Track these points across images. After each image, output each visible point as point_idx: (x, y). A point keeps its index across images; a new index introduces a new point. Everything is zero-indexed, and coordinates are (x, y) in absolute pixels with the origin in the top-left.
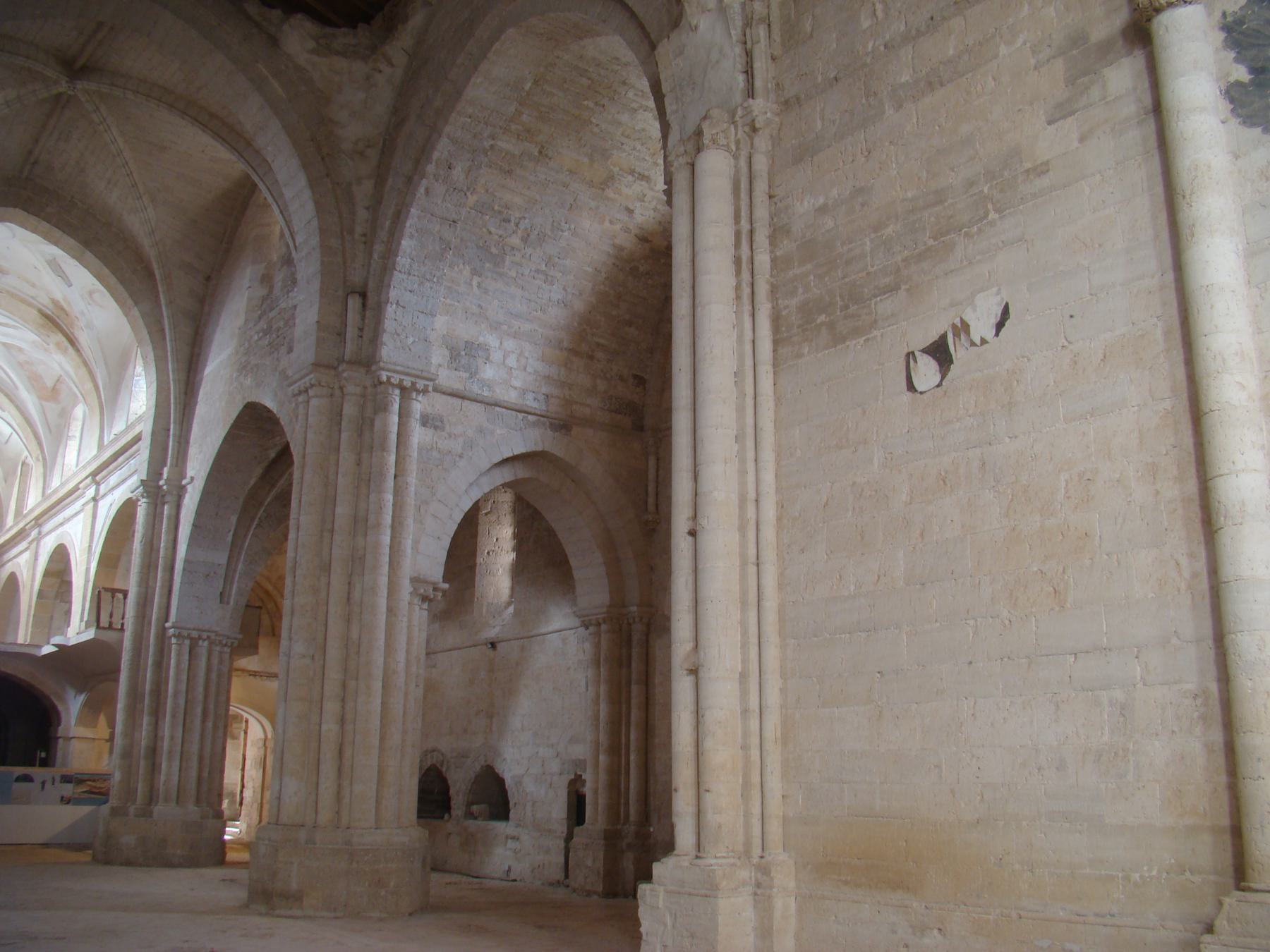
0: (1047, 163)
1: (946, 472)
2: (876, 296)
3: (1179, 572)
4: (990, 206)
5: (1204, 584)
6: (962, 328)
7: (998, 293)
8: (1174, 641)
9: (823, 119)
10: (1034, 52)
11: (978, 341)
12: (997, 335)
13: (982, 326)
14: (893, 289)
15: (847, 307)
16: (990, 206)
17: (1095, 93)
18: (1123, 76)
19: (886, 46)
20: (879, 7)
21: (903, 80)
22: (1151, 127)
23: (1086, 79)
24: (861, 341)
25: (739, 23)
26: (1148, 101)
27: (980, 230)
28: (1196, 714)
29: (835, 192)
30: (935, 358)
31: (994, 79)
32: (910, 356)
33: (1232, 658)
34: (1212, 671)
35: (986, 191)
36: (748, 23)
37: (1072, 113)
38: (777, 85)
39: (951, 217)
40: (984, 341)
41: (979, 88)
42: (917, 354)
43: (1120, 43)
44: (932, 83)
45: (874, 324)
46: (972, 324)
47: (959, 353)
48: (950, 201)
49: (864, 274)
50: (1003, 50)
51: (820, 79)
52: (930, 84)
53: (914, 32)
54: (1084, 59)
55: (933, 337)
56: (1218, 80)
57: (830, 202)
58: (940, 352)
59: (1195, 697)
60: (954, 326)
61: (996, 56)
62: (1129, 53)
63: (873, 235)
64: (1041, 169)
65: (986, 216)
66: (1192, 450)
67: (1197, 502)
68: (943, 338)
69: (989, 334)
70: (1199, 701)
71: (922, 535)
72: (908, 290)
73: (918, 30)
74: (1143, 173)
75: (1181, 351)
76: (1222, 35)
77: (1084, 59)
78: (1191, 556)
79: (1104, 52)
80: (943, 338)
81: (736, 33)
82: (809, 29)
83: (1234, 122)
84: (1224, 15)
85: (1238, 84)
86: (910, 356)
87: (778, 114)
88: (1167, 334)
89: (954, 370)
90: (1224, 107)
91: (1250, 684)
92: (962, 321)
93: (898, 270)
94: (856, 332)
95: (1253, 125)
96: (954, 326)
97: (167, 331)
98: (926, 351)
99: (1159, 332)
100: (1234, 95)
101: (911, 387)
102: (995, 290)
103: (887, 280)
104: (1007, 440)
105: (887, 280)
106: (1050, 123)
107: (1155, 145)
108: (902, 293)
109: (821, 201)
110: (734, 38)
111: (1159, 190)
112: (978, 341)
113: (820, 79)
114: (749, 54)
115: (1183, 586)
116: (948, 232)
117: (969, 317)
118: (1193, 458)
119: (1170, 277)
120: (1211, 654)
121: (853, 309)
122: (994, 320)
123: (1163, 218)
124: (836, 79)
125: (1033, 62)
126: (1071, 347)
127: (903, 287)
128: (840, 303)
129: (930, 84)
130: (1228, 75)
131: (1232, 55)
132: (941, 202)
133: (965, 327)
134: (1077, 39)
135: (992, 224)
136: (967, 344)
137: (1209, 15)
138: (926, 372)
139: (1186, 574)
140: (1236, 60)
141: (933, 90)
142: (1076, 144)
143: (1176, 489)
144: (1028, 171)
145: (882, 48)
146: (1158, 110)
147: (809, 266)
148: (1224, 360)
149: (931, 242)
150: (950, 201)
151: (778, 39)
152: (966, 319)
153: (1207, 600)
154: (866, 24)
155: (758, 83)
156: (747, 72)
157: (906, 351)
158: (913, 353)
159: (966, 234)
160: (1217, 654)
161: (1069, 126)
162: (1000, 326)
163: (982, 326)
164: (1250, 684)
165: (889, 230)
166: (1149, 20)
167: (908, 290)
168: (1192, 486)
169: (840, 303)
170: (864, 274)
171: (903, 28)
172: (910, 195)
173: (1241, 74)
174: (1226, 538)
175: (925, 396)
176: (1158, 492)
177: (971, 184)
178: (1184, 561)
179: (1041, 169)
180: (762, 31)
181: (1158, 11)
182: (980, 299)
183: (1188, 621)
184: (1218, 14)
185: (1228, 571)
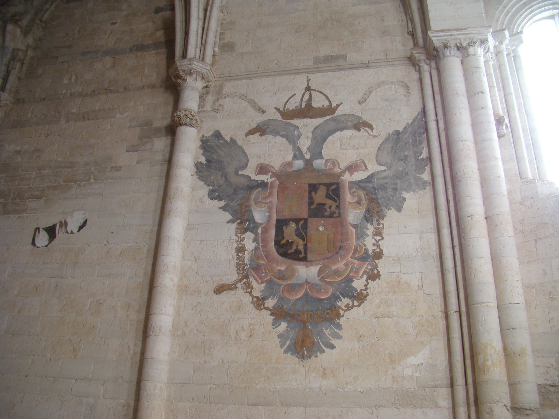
0: (121, 167)
1: (39, 285)
2: (30, 198)
3: (129, 351)
4: (92, 176)
5: (138, 359)
6: (64, 224)
7: (84, 214)
8: (120, 380)
9: (32, 113)
10: (130, 121)
11: (69, 231)
12: (79, 231)
13: (73, 226)
14: (39, 198)
15: (15, 199)
16: (92, 176)
17: (148, 146)
18: (161, 144)
19: (71, 94)
20: (74, 77)
21: (73, 111)
22: (165, 167)
23: (146, 140)
24: (17, 216)
25: (9, 57)
26: (167, 157)
27: (85, 185)
28: (122, 414)
29: (26, 147)
30: (48, 233)
31: (111, 125)
32: (37, 229)
33: (142, 391)
34: (133, 396)
35: (92, 169)
36: (13, 58)
37: (137, 151)
38: (17, 91)
39: (75, 175)
40: (72, 232)
41: (103, 127)
42: (41, 229)
43: (164, 131)
44: (85, 117)
45: (25, 211)
46: (69, 223)
47: (60, 234)
48: (76, 168)
49: (27, 187)
50: (118, 115)
51: (37, 96)
52: (84, 117)
53: (84, 94)
54: (148, 132)
55: (50, 224)
56: (194, 159)
57: (23, 150)
58: (51, 232)
59: (123, 406)
60: (61, 222)
61: (115, 117)
62: (166, 136)
63: (37, 172)
64: (118, 169)
65: (89, 180)
66: (146, 300)
67: (143, 323)
68: (55, 226)
69: (75, 230)
70: (125, 408)
71: (19, 312)
72: (45, 200)
73: (86, 93)
74: (157, 183)
75: (152, 259)
76: (200, 143)
77: (148, 132)
78: (135, 345)
79: (157, 132)
80: (55, 226)
81: (5, 61)
82: (40, 73)
83: (196, 177)
84: (203, 136)
85: (201, 163)
86: (37, 229)
87: (12, 104)
88: (148, 251)
89: (55, 241)
90: (194, 170)
91: (147, 403)
92: (65, 221)
93: (44, 190)
94: (15, 212)
95: (201, 180)
96: (61, 222)
97: (520, 129)
98: (46, 229)
99: (145, 249)
100: (198, 166)
101: (33, 243)
102: (83, 212)
103: (37, 193)
104: (70, 278)
105: (37, 193)
106: (127, 151)
107: (165, 175)
108: (42, 201)
109: (19, 148)
110: (4, 62)
111: (161, 193)
112: (69, 231)
113: (37, 96)
114: (8, 72)
115: (129, 357)
116: (71, 181)
117: (69, 220)
118: (146, 304)
119: (156, 228)
120: (134, 389)
121: (18, 201)
122: (79, 225)
123: (160, 204)
124: (44, 99)
125: (128, 125)
126: (108, 245)
127: (44, 198)
128: (12, 196)
129: (84, 117)
130: (199, 158)
131: (202, 152)
132: (72, 168)
133: (66, 224)
134: (148, 123)
135: (91, 184)
136: (64, 232)
137: (198, 134)
138: (43, 239)
139: (132, 352)
140: (203, 154)
141: (84, 120)
142: (135, 163)
143: (136, 316)
144: (112, 167)
145: (69, 95)
146: (170, 162)
147: (3, 175)
148: (167, 268)
149: (62, 183)
150: (76, 168)
151: (24, 72)
152: (67, 220)
153: (137, 366)
154: (65, 82)
155: (8, 86)
156: (4, 79)
157: (36, 226)
158: (39, 228)
159: (79, 185)
160: (136, 389)
161: (135, 155)
162: (81, 228)
163: (73, 226)
164: (147, 403)
165: (46, 172)
166: (176, 127)
167: (45, 200)
168: (142, 316)
169: (12, 196)
170: (27, 187)
171: (80, 90)
172: (59, 160)
173: (203, 160)
174: (150, 340)
175: (38, 249)
176: (128, 316)
177: (87, 164)
178: (132, 347)
179: (118, 169)
180: (18, 65)
181: (181, 125)
182: (76, 213)
183: (128, 372)
184: (201, 135)
185: (148, 354)
